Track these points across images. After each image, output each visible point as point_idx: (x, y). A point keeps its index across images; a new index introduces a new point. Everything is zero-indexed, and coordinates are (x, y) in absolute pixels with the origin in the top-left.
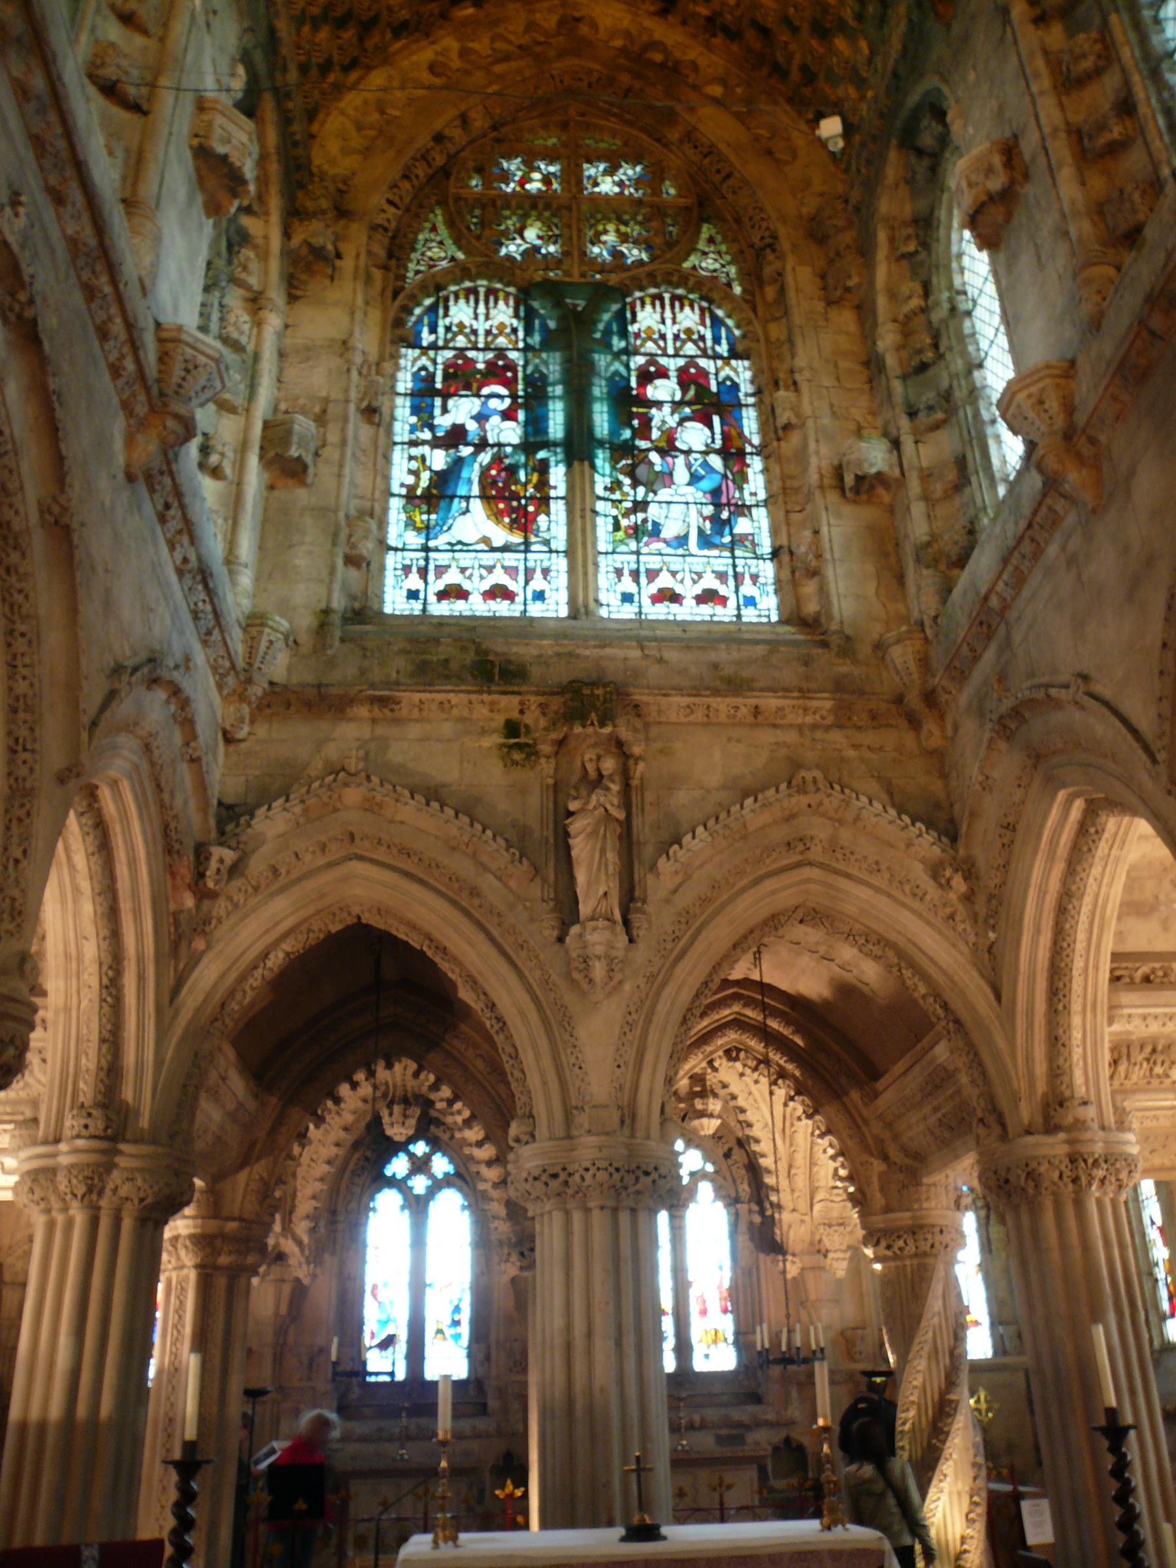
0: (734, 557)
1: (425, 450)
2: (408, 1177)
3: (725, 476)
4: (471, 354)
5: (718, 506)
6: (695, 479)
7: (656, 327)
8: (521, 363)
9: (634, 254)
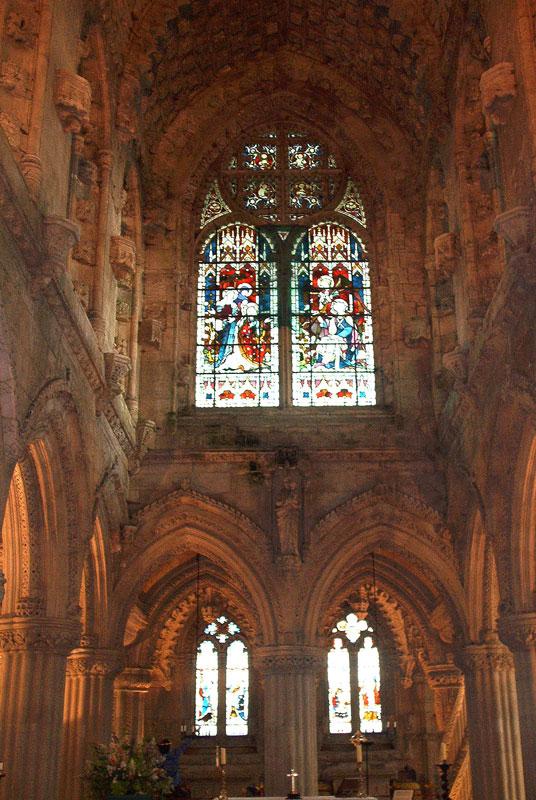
0: (356, 372)
1: (212, 320)
2: (216, 634)
3: (354, 328)
4: (233, 265)
5: (350, 345)
6: (339, 330)
7: (323, 244)
8: (257, 269)
9: (313, 202)
